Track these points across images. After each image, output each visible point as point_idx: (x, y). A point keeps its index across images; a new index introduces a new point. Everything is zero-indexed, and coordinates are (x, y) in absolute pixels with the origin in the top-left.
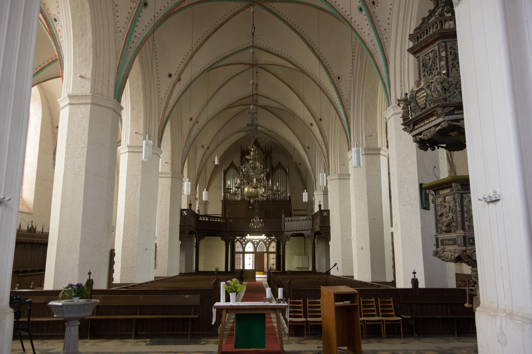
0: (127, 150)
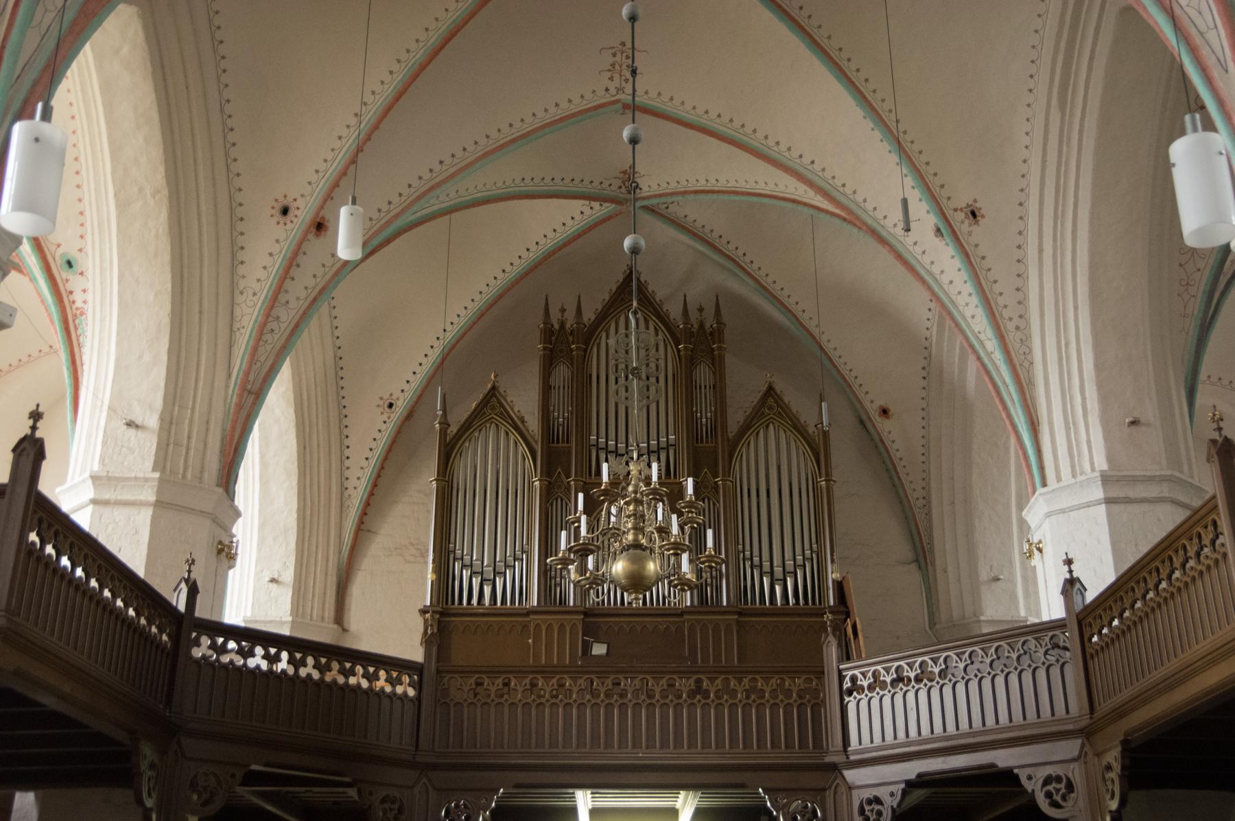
0: (89, 493)
